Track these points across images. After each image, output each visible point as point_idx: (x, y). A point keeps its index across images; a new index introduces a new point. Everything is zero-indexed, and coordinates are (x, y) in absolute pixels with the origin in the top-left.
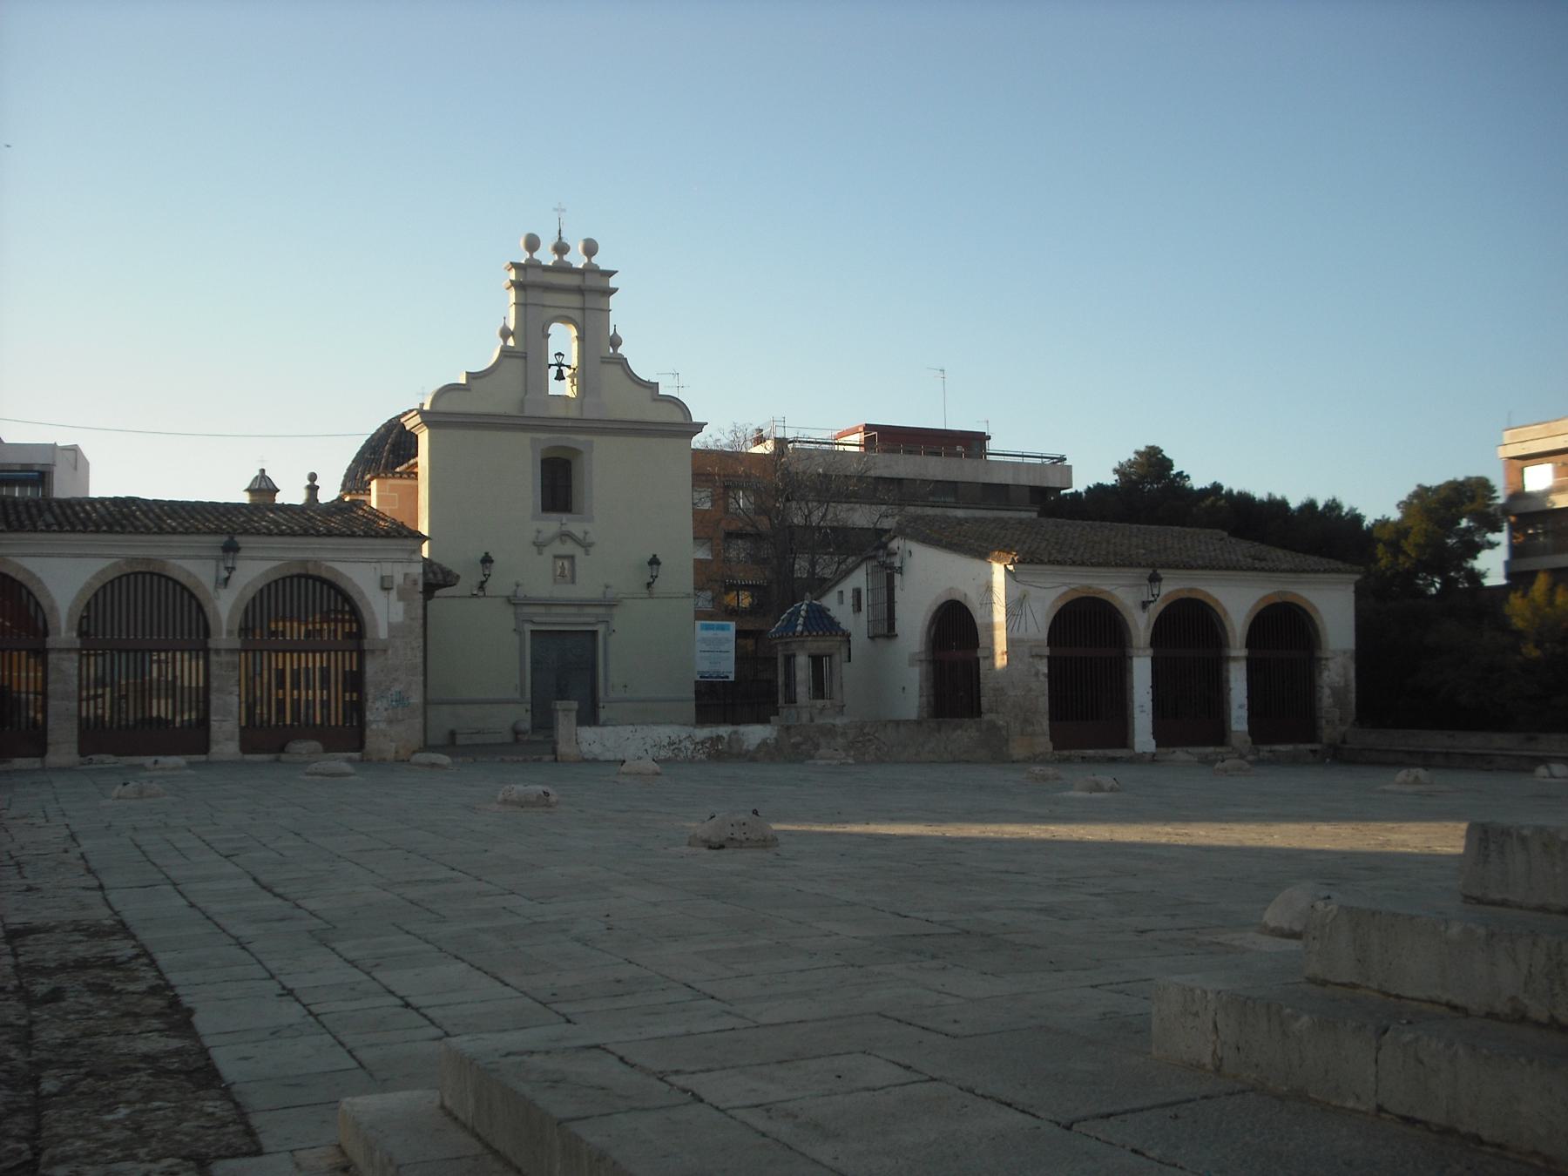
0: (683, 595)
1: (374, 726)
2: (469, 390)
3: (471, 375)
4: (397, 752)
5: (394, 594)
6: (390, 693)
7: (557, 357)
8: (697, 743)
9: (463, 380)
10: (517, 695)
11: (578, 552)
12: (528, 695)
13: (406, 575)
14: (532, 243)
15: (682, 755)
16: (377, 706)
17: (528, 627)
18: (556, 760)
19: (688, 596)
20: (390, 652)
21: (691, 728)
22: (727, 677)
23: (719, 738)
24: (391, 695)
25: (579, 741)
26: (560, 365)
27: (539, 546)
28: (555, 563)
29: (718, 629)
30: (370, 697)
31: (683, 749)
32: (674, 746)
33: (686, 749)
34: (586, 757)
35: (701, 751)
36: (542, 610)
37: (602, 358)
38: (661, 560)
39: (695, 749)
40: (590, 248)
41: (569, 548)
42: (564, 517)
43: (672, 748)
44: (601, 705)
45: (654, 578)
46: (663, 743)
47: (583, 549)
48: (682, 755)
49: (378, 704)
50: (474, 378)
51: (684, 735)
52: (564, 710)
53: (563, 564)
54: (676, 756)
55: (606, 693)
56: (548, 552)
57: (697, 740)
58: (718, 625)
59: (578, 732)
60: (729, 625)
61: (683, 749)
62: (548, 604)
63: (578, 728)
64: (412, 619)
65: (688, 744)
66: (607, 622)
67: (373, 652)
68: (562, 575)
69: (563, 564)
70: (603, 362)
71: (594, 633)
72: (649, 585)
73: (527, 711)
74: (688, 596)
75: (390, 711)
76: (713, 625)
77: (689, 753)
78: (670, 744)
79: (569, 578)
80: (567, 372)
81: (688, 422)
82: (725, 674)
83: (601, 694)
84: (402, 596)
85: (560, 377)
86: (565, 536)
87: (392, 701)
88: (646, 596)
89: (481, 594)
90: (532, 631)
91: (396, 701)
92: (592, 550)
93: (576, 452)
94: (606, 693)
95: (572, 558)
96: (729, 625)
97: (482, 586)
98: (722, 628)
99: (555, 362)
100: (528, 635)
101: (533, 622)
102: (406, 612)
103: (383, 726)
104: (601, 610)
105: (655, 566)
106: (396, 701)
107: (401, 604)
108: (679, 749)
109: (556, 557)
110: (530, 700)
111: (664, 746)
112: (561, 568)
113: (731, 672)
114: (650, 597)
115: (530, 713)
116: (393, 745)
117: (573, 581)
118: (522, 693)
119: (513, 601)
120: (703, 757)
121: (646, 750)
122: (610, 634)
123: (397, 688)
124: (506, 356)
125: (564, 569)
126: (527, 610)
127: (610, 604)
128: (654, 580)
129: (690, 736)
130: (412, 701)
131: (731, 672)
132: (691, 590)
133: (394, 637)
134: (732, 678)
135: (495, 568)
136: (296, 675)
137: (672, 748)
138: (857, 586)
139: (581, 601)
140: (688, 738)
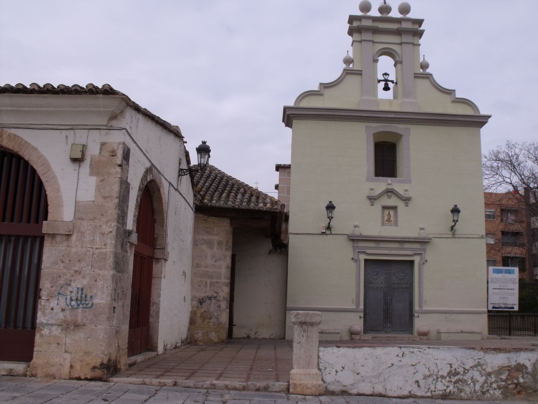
0: (478, 236)
1: (46, 331)
2: (322, 95)
3: (322, 85)
4: (71, 367)
5: (86, 166)
6: (70, 289)
7: (384, 76)
8: (489, 374)
9: (316, 88)
10: (353, 307)
11: (400, 205)
12: (362, 307)
13: (103, 144)
14: (365, 7)
15: (467, 389)
16: (51, 305)
17: (363, 257)
18: (288, 390)
19: (482, 237)
20: (74, 238)
21: (481, 354)
22: (513, 308)
23: (520, 368)
24: (71, 292)
25: (321, 367)
26: (386, 80)
27: (372, 199)
28: (383, 212)
29: (506, 273)
30: (44, 294)
31: (470, 381)
32: (456, 378)
33: (474, 382)
34: (331, 388)
35: (494, 386)
36: (373, 245)
37: (415, 74)
38: (460, 209)
39: (485, 382)
40: (405, 9)
41: (392, 201)
42: (389, 180)
43: (454, 379)
44: (416, 315)
45: (455, 221)
46: (441, 373)
47: (404, 202)
48: (467, 389)
49: (53, 303)
50: (325, 87)
51: (470, 363)
52: (302, 324)
53: (389, 212)
54: (461, 391)
55: (420, 306)
56: (378, 205)
57: (489, 370)
58: (506, 270)
59: (320, 354)
60: (514, 270)
61: (470, 381)
62: (377, 240)
63: (321, 349)
64: (105, 198)
65: (476, 374)
66: (421, 254)
67: (53, 236)
68: (389, 220)
69: (389, 212)
70: (415, 77)
71: (412, 262)
72: (452, 228)
73: (360, 318)
74: (482, 237)
75: (67, 312)
76: (502, 270)
77: (478, 387)
78: (450, 374)
79: (393, 222)
80: (391, 85)
81: (477, 114)
82: (511, 306)
83: (416, 307)
84: (95, 170)
85: (386, 88)
86: (390, 192)
87: (71, 300)
88: (451, 236)
89: (328, 232)
90: (366, 260)
91: (77, 300)
92: (410, 203)
93: (399, 136)
94: (420, 306)
95: (395, 208)
96: (514, 270)
97: (329, 228)
98: (509, 272)
99: (383, 79)
100: (362, 263)
101: (365, 253)
102: (98, 189)
103: (56, 331)
104: (417, 246)
105: (456, 214)
106: (77, 300)
107: (93, 180)
108: (464, 382)
109: (384, 208)
110: (363, 310)
111: (443, 377)
112: (388, 215)
113: (515, 304)
114: (453, 237)
115: (362, 320)
116: (67, 356)
117: (396, 224)
118: (358, 304)
119: (354, 239)
120: (498, 393)
121: (417, 382)
122: (423, 263)
123: (76, 285)
124: (347, 73)
125: (390, 216)
126: (361, 244)
127: (424, 242)
128: (455, 223)
129: (479, 364)
130: (96, 301)
131: (515, 304)
132: (484, 233)
133: (82, 219)
134: (516, 308)
135: (335, 212)
136: (211, 283)
137: (454, 379)
138: (515, 308)
139: (403, 238)
140: (476, 366)
